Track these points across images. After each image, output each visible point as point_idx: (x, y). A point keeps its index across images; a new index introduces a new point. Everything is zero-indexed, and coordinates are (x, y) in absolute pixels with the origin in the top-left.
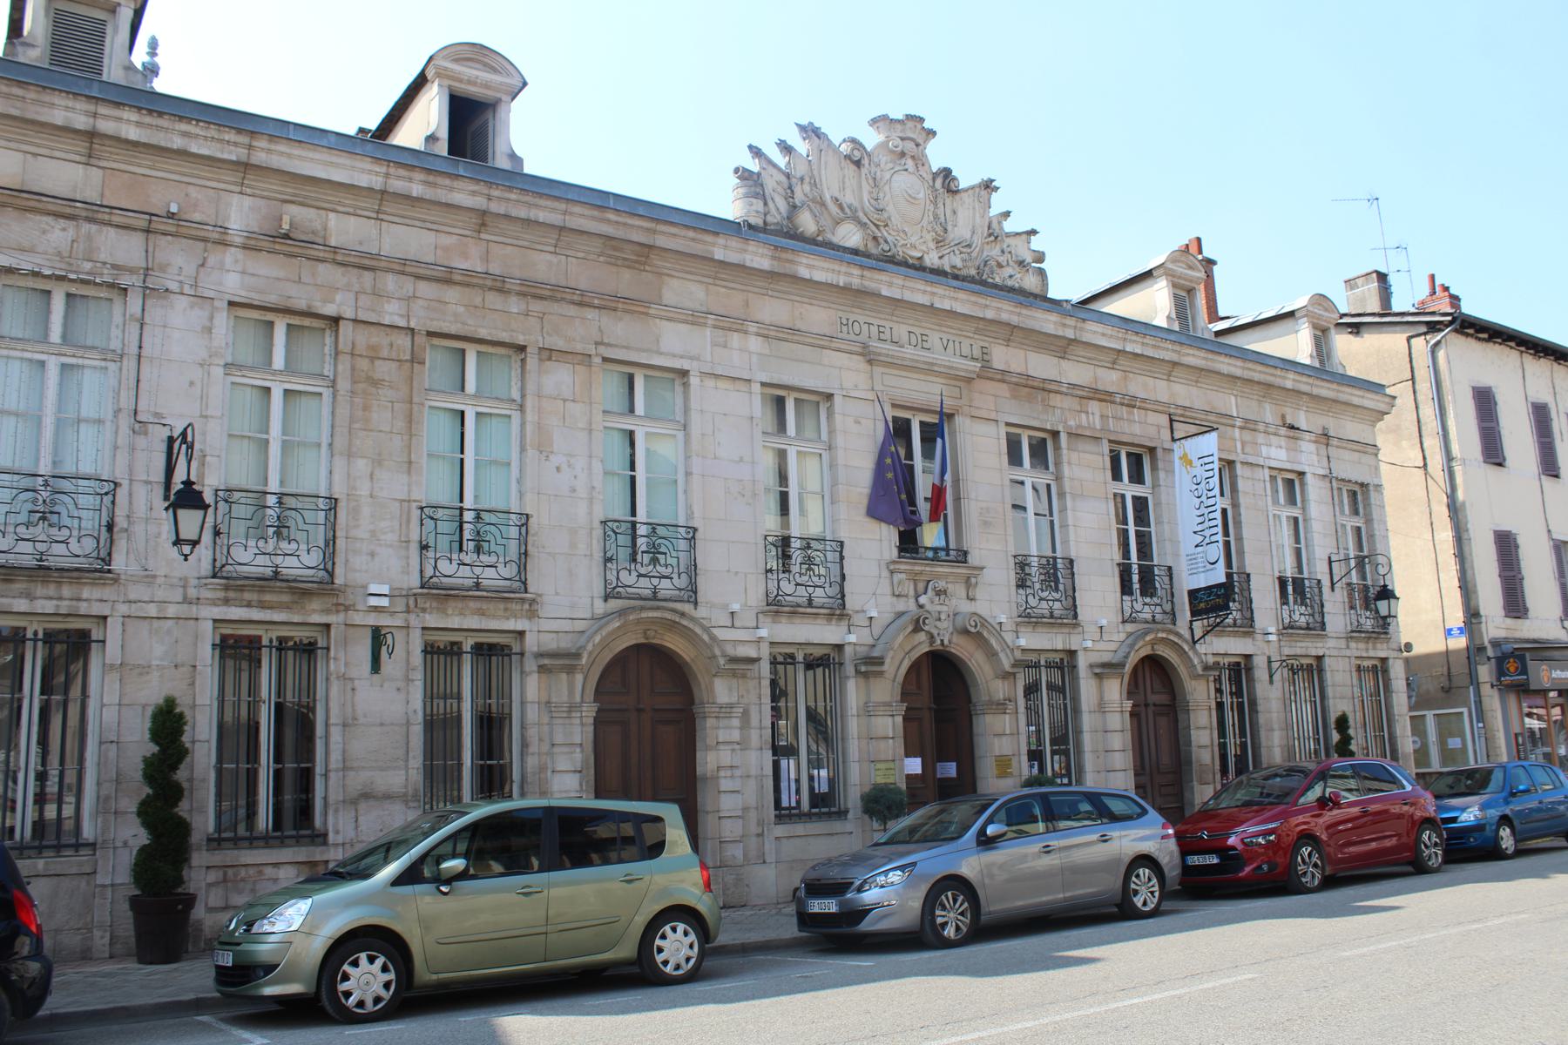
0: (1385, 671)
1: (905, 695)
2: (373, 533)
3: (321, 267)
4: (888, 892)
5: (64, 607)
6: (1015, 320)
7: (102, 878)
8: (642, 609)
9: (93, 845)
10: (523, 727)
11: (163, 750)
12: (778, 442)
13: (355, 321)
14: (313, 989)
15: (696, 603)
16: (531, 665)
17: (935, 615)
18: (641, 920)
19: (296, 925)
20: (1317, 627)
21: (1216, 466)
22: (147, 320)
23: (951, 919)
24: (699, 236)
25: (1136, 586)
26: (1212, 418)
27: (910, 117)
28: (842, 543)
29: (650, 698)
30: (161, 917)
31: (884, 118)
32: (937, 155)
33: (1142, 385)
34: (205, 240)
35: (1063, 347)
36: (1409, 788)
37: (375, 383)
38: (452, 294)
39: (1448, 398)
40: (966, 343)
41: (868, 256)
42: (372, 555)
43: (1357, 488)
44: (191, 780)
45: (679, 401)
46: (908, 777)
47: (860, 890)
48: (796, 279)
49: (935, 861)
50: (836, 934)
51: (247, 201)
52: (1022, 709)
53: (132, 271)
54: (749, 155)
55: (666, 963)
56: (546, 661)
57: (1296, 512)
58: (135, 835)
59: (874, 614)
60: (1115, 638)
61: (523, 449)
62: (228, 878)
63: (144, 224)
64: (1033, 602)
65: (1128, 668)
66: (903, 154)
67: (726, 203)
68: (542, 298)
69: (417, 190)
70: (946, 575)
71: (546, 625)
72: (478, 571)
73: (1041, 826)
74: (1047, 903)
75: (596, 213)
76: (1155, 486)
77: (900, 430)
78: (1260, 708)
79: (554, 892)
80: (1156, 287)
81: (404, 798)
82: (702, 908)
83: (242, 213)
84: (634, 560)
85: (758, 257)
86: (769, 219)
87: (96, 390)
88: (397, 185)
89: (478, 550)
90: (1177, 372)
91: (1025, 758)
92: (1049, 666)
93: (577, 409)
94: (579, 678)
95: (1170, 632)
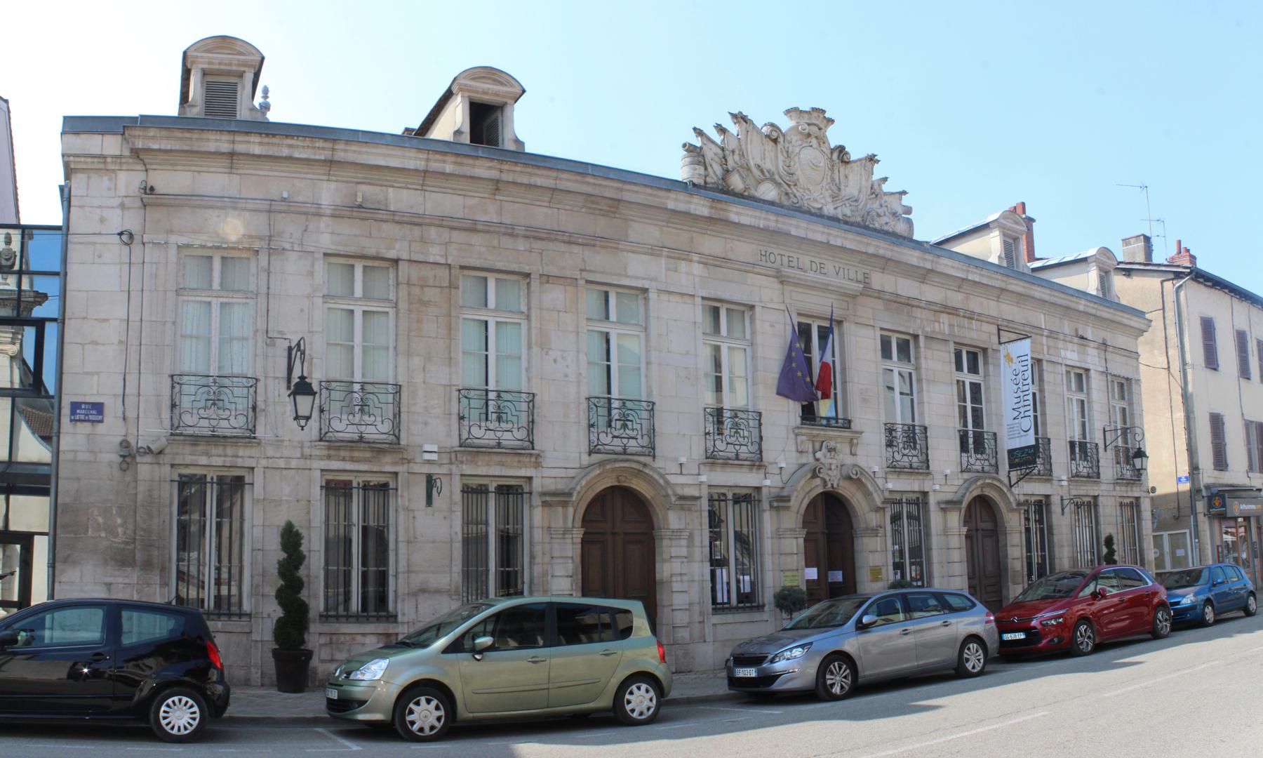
0: (1138, 506)
1: (805, 523)
3: (385, 226)
4: (793, 663)
5: (229, 461)
6: (889, 254)
7: (256, 636)
8: (616, 461)
9: (249, 615)
10: (531, 544)
11: (290, 556)
12: (714, 341)
13: (409, 261)
14: (390, 718)
15: (654, 457)
16: (537, 501)
18: (615, 682)
19: (379, 677)
20: (1095, 476)
21: (1029, 363)
22: (272, 269)
23: (838, 680)
25: (971, 446)
26: (1028, 329)
27: (815, 110)
28: (760, 414)
29: (620, 526)
30: (292, 667)
31: (796, 110)
32: (834, 137)
33: (978, 304)
34: (306, 214)
35: (924, 275)
36: (1150, 584)
37: (425, 303)
38: (476, 239)
39: (1185, 323)
40: (853, 270)
41: (782, 206)
42: (426, 424)
43: (1123, 381)
44: (308, 576)
45: (642, 309)
46: (808, 581)
47: (772, 661)
48: (727, 222)
49: (826, 642)
50: (758, 693)
51: (333, 185)
52: (889, 533)
54: (693, 134)
55: (633, 711)
56: (548, 498)
57: (1082, 396)
58: (275, 611)
59: (783, 465)
60: (956, 483)
61: (530, 347)
62: (333, 641)
63: (267, 207)
64: (898, 457)
65: (965, 504)
66: (809, 135)
67: (677, 168)
68: (541, 239)
69: (449, 168)
70: (836, 438)
71: (547, 473)
72: (499, 434)
73: (901, 616)
75: (578, 178)
76: (986, 375)
77: (803, 332)
78: (1055, 532)
79: (554, 661)
80: (991, 235)
81: (449, 593)
82: (657, 673)
83: (329, 193)
84: (610, 426)
85: (700, 206)
86: (708, 180)
87: (242, 318)
88: (435, 166)
89: (499, 419)
91: (891, 568)
92: (908, 503)
94: (571, 510)
95: (994, 478)
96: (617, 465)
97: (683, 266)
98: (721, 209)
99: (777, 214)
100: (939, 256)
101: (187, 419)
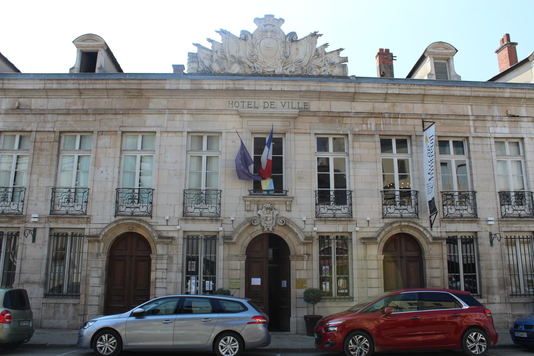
2: (37, 198)
3: (28, 116)
6: (318, 89)
13: (36, 131)
15: (151, 217)
17: (265, 218)
24: (158, 82)
27: (266, 16)
33: (401, 108)
37: (41, 150)
38: (69, 118)
42: (36, 205)
51: (8, 100)
60: (378, 225)
68: (101, 114)
69: (55, 86)
71: (92, 226)
72: (461, 212)
74: (159, 346)
75: (117, 82)
81: (39, 283)
88: (48, 86)
90: (426, 99)
93: (111, 151)
94: (102, 244)
96: (125, 222)
97: (178, 117)
98: (198, 84)
99: (232, 80)
100: (360, 83)
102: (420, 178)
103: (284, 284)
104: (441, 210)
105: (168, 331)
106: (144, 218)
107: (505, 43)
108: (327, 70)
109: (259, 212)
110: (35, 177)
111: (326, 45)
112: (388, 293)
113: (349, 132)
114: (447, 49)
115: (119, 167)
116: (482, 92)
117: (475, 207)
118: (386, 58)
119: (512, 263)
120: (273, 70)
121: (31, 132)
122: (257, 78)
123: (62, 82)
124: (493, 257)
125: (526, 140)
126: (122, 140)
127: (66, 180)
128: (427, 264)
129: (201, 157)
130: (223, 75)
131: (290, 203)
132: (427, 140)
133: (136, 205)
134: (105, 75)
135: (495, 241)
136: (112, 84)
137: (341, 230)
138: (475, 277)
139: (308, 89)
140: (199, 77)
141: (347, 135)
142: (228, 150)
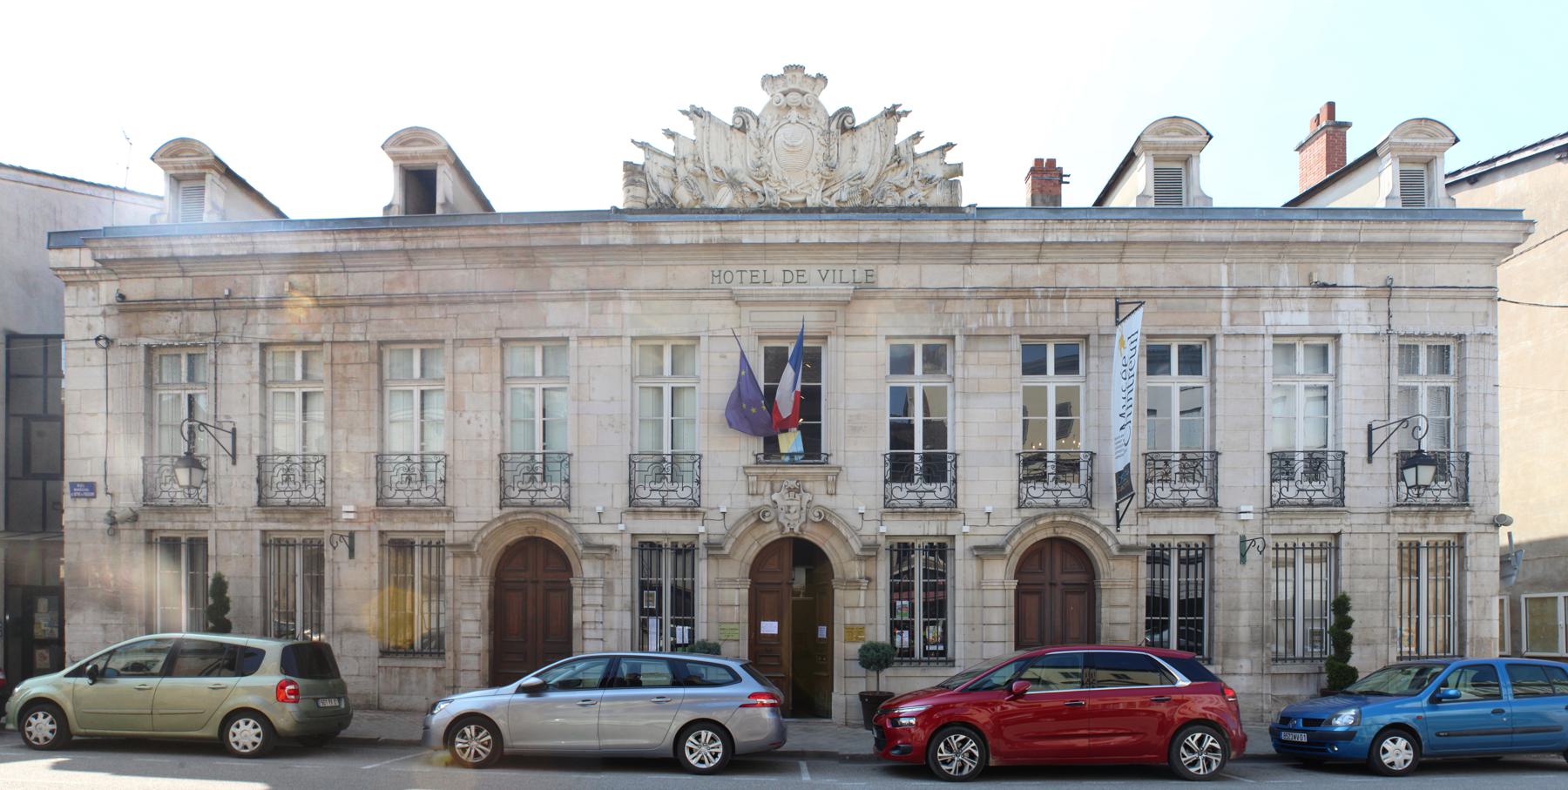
6: (896, 237)
13: (332, 342)
27: (788, 68)
33: (1071, 276)
37: (347, 380)
38: (394, 313)
42: (348, 488)
51: (268, 279)
53: (209, 335)
68: (456, 303)
69: (356, 246)
71: (457, 526)
72: (1184, 494)
75: (480, 231)
90: (1129, 252)
93: (482, 378)
94: (479, 560)
98: (647, 233)
100: (984, 221)
101: (514, 493)
102: (1102, 427)
103: (822, 632)
104: (1141, 490)
105: (589, 719)
106: (556, 511)
107: (1323, 124)
108: (918, 195)
109: (775, 497)
110: (340, 433)
111: (917, 137)
112: (1021, 653)
113: (956, 332)
114: (1187, 134)
115: (502, 412)
116: (1258, 232)
117: (1213, 487)
118: (1047, 177)
119: (1282, 598)
120: (801, 198)
121: (322, 343)
122: (770, 216)
123: (368, 235)
124: (1245, 586)
125: (1345, 340)
126: (502, 358)
127: (401, 440)
128: (1104, 598)
129: (660, 389)
130: (697, 212)
131: (833, 479)
132: (1122, 344)
133: (539, 486)
134: (455, 220)
135: (1252, 554)
136: (472, 239)
137: (933, 531)
138: (1200, 624)
139: (874, 239)
140: (648, 217)
141: (953, 338)
142: (715, 378)
